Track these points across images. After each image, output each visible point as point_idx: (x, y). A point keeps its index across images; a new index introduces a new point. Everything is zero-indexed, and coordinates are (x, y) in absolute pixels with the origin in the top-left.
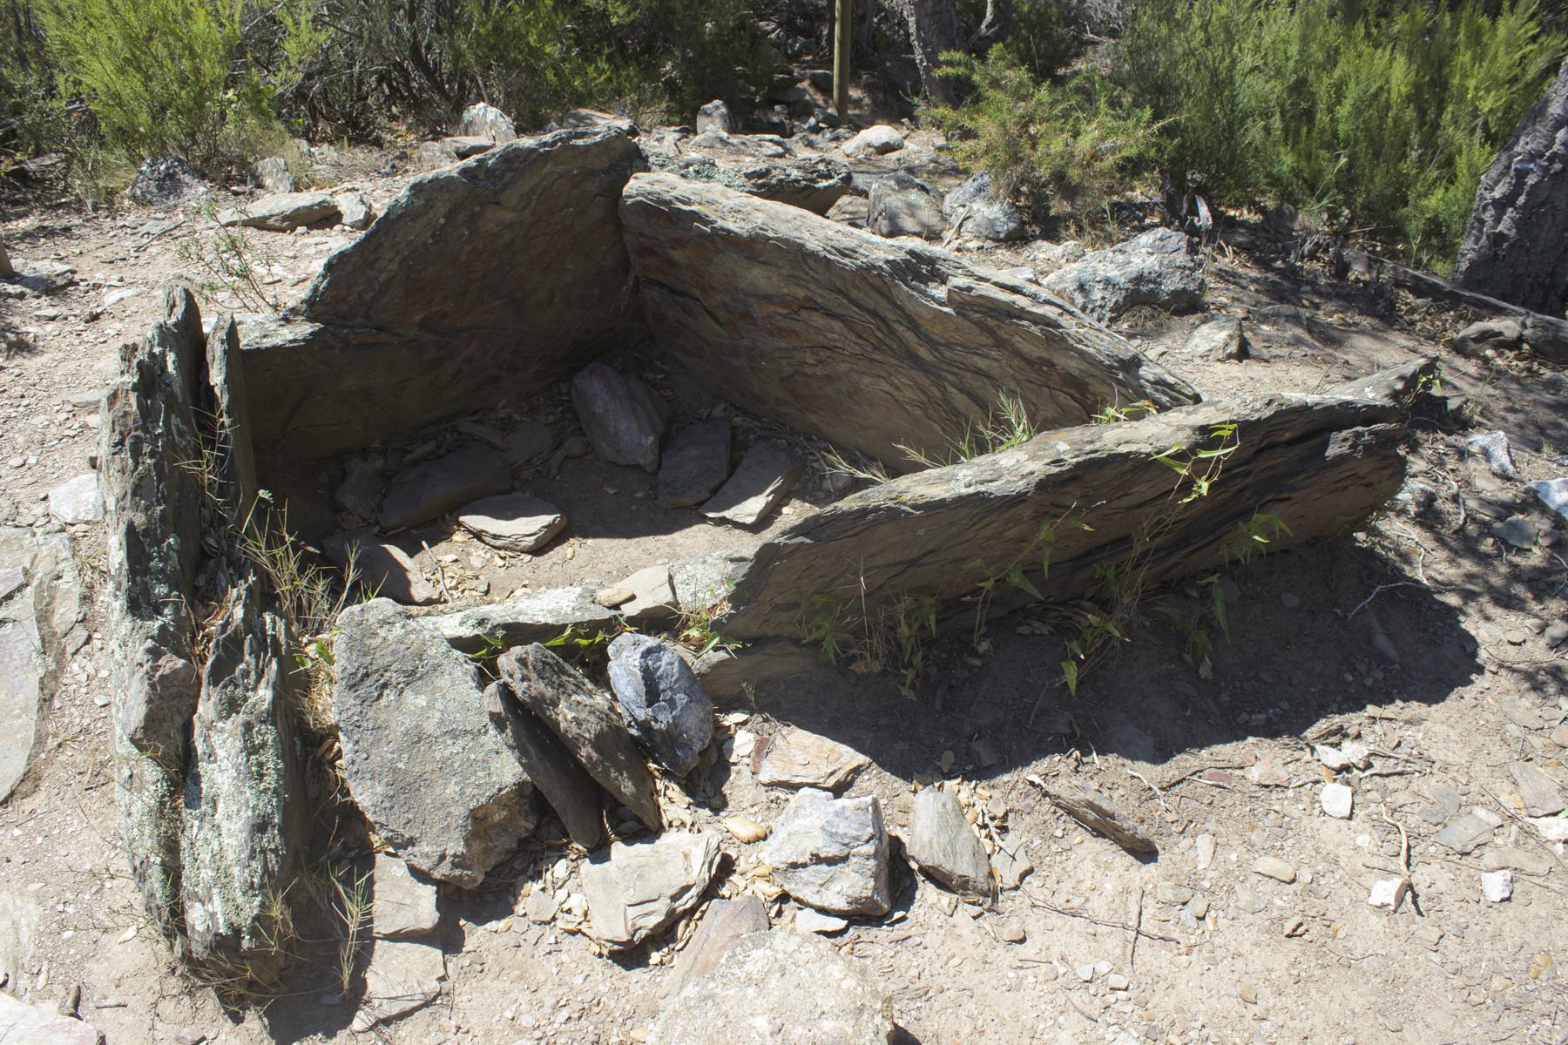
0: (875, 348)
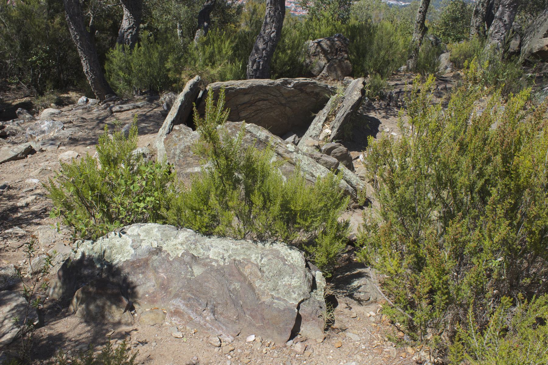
0: (274, 104)
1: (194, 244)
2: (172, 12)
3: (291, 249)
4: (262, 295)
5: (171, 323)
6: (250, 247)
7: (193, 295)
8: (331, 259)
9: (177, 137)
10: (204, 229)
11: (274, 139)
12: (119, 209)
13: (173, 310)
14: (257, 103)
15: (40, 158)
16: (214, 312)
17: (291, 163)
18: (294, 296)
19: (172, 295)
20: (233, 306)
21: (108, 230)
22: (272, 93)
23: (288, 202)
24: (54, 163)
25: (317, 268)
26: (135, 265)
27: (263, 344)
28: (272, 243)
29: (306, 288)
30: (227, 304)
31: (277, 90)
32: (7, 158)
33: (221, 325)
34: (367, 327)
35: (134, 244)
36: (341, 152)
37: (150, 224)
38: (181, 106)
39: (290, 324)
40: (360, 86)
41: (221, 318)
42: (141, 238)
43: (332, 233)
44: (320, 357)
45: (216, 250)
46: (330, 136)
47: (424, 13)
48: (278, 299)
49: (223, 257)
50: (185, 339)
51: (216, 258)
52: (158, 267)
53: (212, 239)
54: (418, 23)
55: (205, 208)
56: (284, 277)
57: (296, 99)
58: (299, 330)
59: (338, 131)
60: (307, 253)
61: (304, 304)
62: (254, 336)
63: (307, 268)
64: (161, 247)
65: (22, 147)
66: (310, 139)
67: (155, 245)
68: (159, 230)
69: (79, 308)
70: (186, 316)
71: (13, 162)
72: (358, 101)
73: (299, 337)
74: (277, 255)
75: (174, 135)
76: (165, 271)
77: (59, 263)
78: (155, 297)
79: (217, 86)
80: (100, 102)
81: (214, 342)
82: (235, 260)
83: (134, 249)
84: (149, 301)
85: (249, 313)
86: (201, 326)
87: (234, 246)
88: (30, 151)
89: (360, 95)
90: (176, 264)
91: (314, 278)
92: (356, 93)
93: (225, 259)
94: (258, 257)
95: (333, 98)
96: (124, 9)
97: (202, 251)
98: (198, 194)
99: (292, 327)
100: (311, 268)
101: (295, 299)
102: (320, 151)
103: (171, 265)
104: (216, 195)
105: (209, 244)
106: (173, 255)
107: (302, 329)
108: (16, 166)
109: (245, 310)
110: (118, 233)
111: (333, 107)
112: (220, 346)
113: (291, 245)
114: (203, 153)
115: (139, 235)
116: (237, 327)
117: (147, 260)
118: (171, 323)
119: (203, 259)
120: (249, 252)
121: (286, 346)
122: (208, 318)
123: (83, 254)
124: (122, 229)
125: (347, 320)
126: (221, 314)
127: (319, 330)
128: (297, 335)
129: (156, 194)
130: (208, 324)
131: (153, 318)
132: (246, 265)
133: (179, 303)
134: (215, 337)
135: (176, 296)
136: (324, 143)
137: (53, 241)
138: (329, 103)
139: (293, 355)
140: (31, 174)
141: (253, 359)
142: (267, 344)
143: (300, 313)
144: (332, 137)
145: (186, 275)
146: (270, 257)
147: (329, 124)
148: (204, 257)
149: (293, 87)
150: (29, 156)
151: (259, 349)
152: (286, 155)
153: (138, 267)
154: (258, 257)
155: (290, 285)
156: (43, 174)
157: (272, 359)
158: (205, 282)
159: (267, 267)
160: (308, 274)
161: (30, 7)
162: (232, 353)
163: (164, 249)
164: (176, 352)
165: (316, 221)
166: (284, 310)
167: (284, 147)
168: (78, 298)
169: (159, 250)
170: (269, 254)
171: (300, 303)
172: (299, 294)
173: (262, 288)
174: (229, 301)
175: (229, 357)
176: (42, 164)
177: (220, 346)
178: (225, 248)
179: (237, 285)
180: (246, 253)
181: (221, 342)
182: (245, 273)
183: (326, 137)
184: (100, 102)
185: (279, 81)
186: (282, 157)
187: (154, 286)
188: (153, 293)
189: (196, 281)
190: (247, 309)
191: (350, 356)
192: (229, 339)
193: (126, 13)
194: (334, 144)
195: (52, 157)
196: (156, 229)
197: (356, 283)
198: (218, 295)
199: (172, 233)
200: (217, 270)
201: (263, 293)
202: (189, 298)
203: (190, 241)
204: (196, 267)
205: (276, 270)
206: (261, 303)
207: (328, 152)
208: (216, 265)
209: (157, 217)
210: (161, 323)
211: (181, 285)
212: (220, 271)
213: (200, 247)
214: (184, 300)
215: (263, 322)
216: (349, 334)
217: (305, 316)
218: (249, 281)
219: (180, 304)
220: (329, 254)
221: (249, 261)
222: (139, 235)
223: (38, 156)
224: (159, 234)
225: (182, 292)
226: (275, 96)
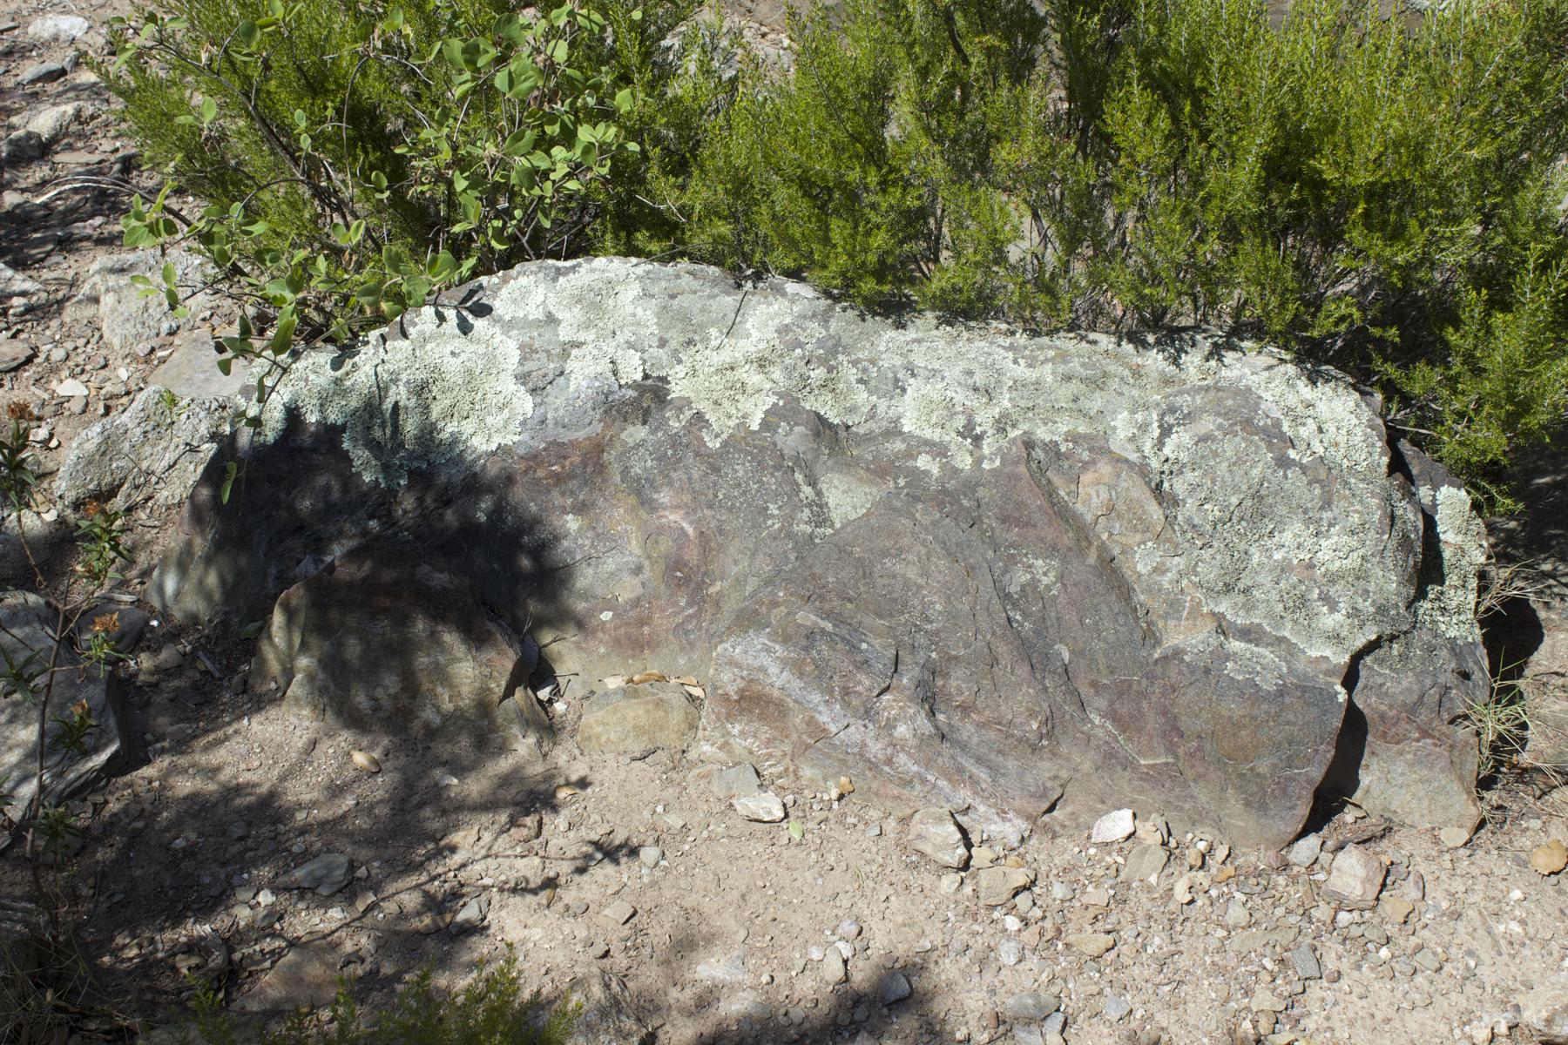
1: (823, 361)
4: (1166, 616)
5: (725, 747)
6: (1105, 374)
7: (827, 615)
12: (450, 183)
13: (732, 690)
16: (930, 700)
18: (1330, 620)
19: (727, 617)
20: (1023, 670)
21: (402, 301)
26: (541, 473)
27: (1172, 855)
28: (1216, 352)
29: (1389, 583)
30: (995, 661)
37: (600, 262)
39: (1309, 762)
41: (967, 730)
42: (565, 334)
44: (1460, 926)
45: (934, 390)
48: (1249, 634)
50: (794, 830)
51: (933, 434)
52: (651, 482)
53: (911, 334)
55: (873, 179)
56: (1281, 525)
61: (1381, 662)
63: (1399, 478)
64: (664, 380)
67: (632, 370)
68: (646, 294)
69: (303, 662)
70: (798, 719)
73: (1349, 815)
76: (686, 498)
77: (193, 450)
78: (642, 622)
81: (940, 848)
82: (1029, 445)
83: (533, 391)
85: (1102, 703)
86: (873, 766)
87: (1022, 371)
91: (1430, 522)
93: (977, 440)
94: (1144, 427)
97: (861, 396)
98: (834, 105)
99: (1317, 773)
100: (1415, 471)
101: (1336, 638)
104: (924, 107)
105: (898, 361)
106: (721, 423)
107: (1365, 778)
109: (1085, 690)
110: (451, 314)
112: (966, 866)
116: (1044, 770)
119: (869, 438)
120: (1096, 403)
121: (1286, 866)
122: (902, 730)
123: (293, 415)
124: (472, 293)
128: (1340, 809)
129: (623, 100)
130: (902, 758)
131: (643, 721)
132: (1086, 465)
134: (940, 820)
135: (748, 620)
137: (165, 327)
141: (1127, 934)
142: (1192, 857)
143: (1359, 703)
145: (789, 520)
146: (1207, 424)
148: (872, 425)
151: (1153, 879)
153: (559, 479)
154: (1144, 427)
155: (1311, 566)
157: (1221, 933)
158: (886, 554)
162: (1023, 901)
163: (677, 390)
164: (754, 897)
165: (1452, 240)
166: (1281, 692)
168: (290, 615)
170: (1203, 410)
171: (1357, 658)
172: (1355, 613)
173: (1166, 581)
174: (1002, 649)
175: (1012, 923)
177: (966, 866)
178: (980, 379)
179: (1043, 571)
180: (1085, 404)
181: (969, 845)
182: (1080, 508)
187: (638, 570)
188: (636, 603)
189: (841, 549)
190: (1094, 684)
192: (1010, 829)
196: (634, 289)
198: (952, 616)
199: (714, 304)
202: (811, 635)
203: (801, 345)
204: (836, 478)
205: (1236, 489)
206: (1165, 659)
208: (935, 471)
213: (852, 374)
214: (786, 639)
215: (1171, 749)
217: (1382, 717)
218: (1103, 548)
219: (766, 660)
220: (1525, 407)
221: (1099, 447)
222: (551, 320)
224: (647, 314)
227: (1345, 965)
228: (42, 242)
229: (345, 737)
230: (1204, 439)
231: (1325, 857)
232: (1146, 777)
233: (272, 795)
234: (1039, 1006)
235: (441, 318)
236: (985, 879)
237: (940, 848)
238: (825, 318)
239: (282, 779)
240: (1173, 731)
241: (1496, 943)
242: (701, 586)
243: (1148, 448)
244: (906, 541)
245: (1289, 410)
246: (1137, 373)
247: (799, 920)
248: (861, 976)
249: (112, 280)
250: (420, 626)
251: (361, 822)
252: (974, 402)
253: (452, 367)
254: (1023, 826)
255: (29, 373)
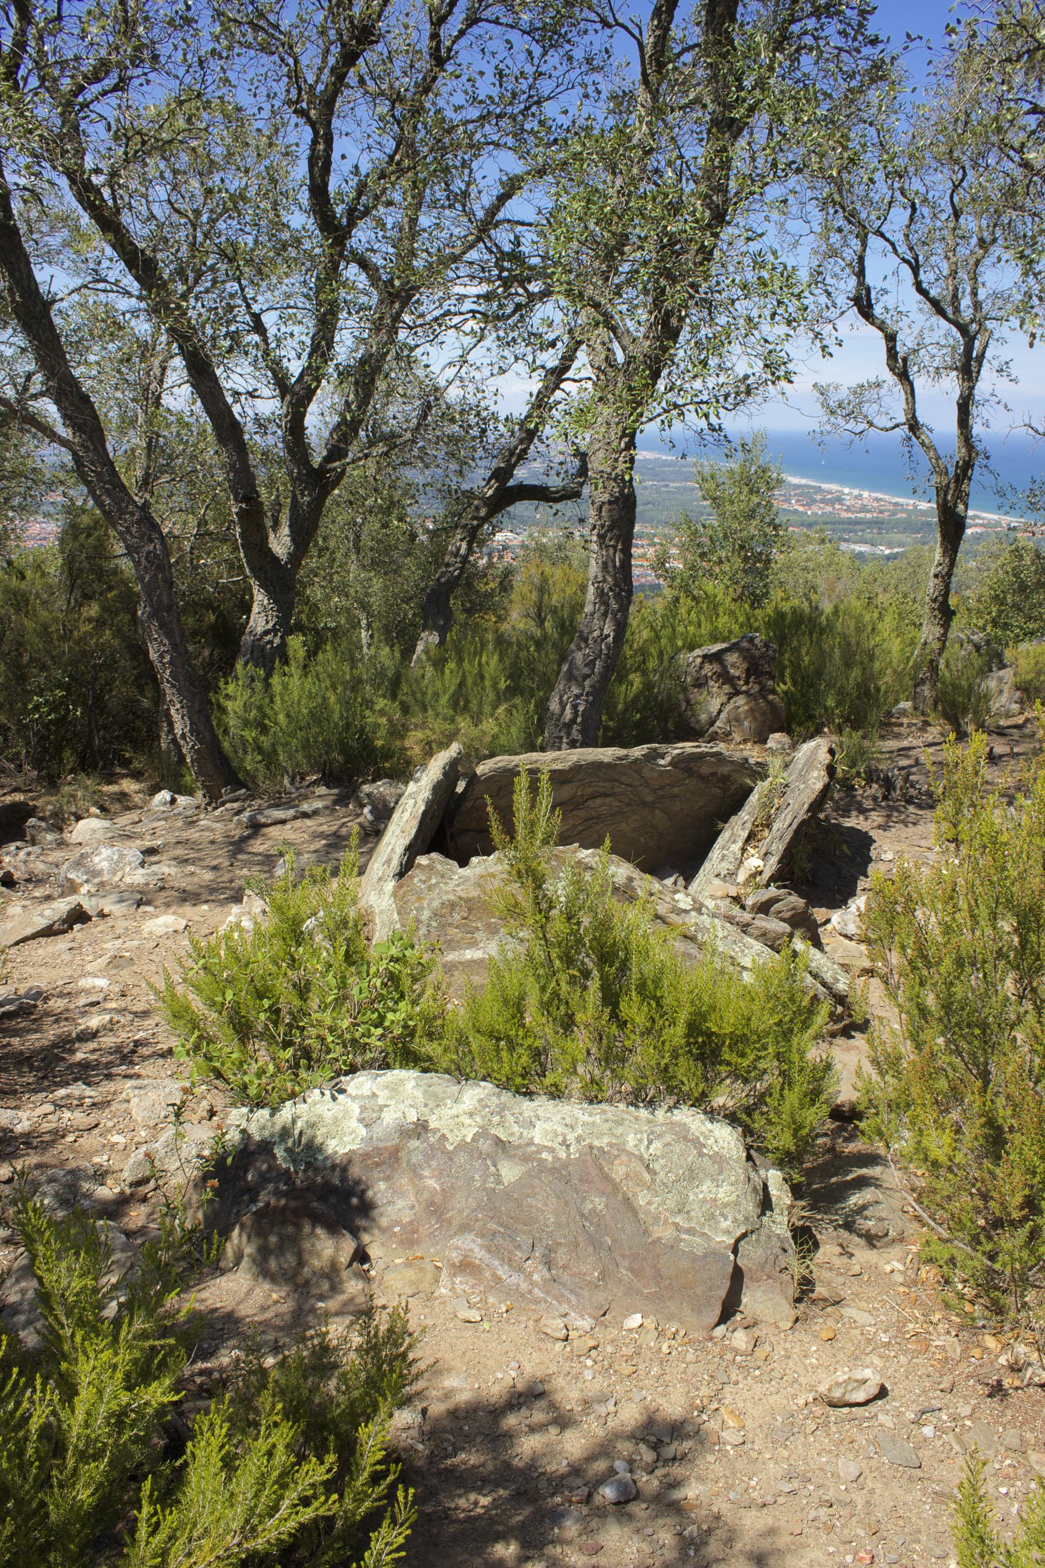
0: (627, 804)
1: (499, 1113)
2: (352, 591)
3: (712, 1120)
5: (452, 1289)
7: (501, 1225)
8: (802, 1139)
9: (424, 882)
10: (519, 1080)
11: (645, 883)
13: (457, 1261)
14: (590, 802)
15: (101, 932)
16: (549, 1264)
17: (685, 937)
18: (725, 1224)
20: (590, 1249)
22: (623, 779)
23: (704, 1017)
24: (136, 943)
25: (769, 1162)
26: (369, 1162)
27: (661, 1334)
28: (670, 1109)
29: (750, 1207)
30: (577, 1245)
31: (636, 771)
32: (29, 931)
33: (567, 1293)
34: (887, 1293)
35: (364, 1115)
36: (793, 909)
37: (396, 1072)
38: (424, 813)
39: (719, 1288)
40: (824, 757)
41: (566, 1277)
43: (801, 1085)
45: (548, 1126)
46: (761, 873)
47: (946, 578)
48: (690, 1231)
49: (564, 1141)
50: (486, 1325)
51: (550, 1144)
53: (536, 1103)
54: (934, 601)
57: (676, 790)
58: (739, 1302)
59: (779, 862)
60: (747, 1131)
61: (748, 1243)
62: (639, 1316)
63: (750, 1163)
65: (62, 907)
66: (717, 882)
67: (412, 1117)
68: (418, 1085)
70: (488, 1274)
71: (43, 940)
72: (822, 791)
73: (738, 1317)
74: (683, 1134)
75: (416, 877)
77: (189, 1162)
78: (414, 1232)
79: (500, 765)
80: (209, 804)
81: (555, 1330)
82: (591, 1147)
83: (366, 1126)
84: (401, 1242)
85: (626, 1264)
86: (522, 1295)
87: (586, 1118)
88: (78, 916)
89: (826, 779)
90: (462, 1158)
91: (765, 1187)
92: (815, 774)
93: (568, 1146)
94: (641, 1141)
95: (761, 788)
96: (256, 590)
97: (516, 1129)
99: (723, 1293)
101: (728, 1232)
102: (743, 907)
103: (451, 1159)
106: (453, 1140)
107: (745, 1300)
108: (50, 949)
109: (619, 1259)
110: (327, 1093)
111: (764, 806)
113: (712, 1114)
114: (514, 911)
115: (374, 1095)
116: (601, 1297)
117: (397, 1150)
118: (452, 1289)
119: (519, 1146)
120: (619, 1131)
121: (711, 1339)
125: (841, 1280)
126: (565, 1267)
127: (784, 1302)
128: (734, 1315)
130: (536, 1290)
132: (616, 1157)
133: (471, 1245)
135: (464, 1228)
136: (749, 890)
137: (163, 1114)
138: (754, 798)
139: (729, 1356)
140: (89, 968)
141: (642, 1367)
142: (669, 1334)
144: (766, 875)
145: (485, 1181)
146: (668, 1138)
147: (756, 847)
149: (670, 764)
150: (77, 927)
152: (674, 918)
154: (641, 1141)
155: (715, 1200)
156: (116, 967)
158: (528, 1196)
159: (661, 1161)
160: (753, 1175)
161: (23, 586)
162: (593, 1353)
163: (432, 1125)
164: (469, 1354)
166: (705, 1256)
167: (668, 899)
169: (421, 1128)
171: (738, 1241)
172: (735, 1220)
173: (652, 1208)
174: (581, 1239)
175: (589, 1362)
176: (108, 945)
177: (566, 1339)
178: (568, 1121)
179: (598, 1202)
180: (615, 1131)
182: (614, 1176)
183: (753, 876)
184: (209, 804)
185: (638, 752)
186: (665, 922)
187: (412, 1207)
188: (411, 1223)
189: (507, 1194)
190: (622, 1255)
191: (857, 1358)
192: (586, 1323)
193: (260, 597)
194: (773, 891)
195: (127, 929)
196: (412, 1083)
197: (855, 1199)
198: (558, 1225)
199: (449, 1090)
200: (553, 1170)
201: (656, 1219)
202: (494, 1234)
205: (682, 1167)
206: (654, 1242)
207: (764, 908)
208: (550, 1159)
209: (409, 1058)
210: (430, 1290)
211: (471, 1202)
212: (559, 1171)
213: (512, 1119)
215: (658, 1284)
216: (849, 1312)
217: (750, 1269)
218: (624, 1193)
219: (473, 1246)
221: (622, 1149)
222: (374, 1095)
223: (97, 927)
224: (419, 1094)
225: (477, 1220)
226: (630, 785)
227: (740, 1378)
228: (97, 1075)
229: (267, 1286)
230: (668, 1144)
231: (728, 1334)
232: (647, 1298)
233: (233, 1311)
234: (603, 1395)
235: (323, 1094)
236: (575, 1343)
237: (555, 1330)
238: (499, 1096)
239: (238, 1303)
240: (658, 1276)
241: (806, 1368)
242: (441, 1215)
243: (643, 1149)
244: (537, 1190)
245: (702, 1133)
246: (637, 1118)
247: (491, 1363)
248: (520, 1386)
249: (137, 1092)
250: (307, 1229)
251: (278, 1322)
252: (566, 1130)
253: (328, 1116)
254: (592, 1321)
255: (96, 1131)
